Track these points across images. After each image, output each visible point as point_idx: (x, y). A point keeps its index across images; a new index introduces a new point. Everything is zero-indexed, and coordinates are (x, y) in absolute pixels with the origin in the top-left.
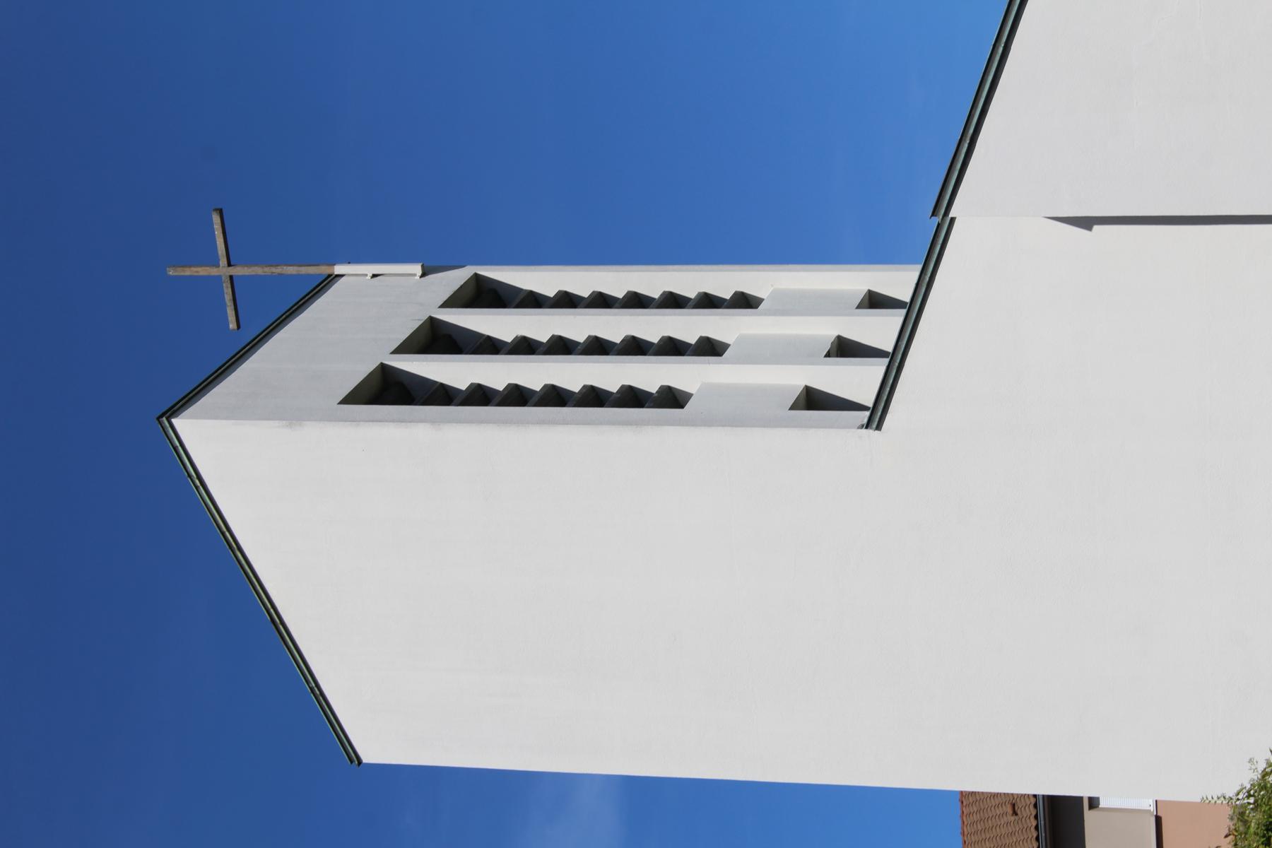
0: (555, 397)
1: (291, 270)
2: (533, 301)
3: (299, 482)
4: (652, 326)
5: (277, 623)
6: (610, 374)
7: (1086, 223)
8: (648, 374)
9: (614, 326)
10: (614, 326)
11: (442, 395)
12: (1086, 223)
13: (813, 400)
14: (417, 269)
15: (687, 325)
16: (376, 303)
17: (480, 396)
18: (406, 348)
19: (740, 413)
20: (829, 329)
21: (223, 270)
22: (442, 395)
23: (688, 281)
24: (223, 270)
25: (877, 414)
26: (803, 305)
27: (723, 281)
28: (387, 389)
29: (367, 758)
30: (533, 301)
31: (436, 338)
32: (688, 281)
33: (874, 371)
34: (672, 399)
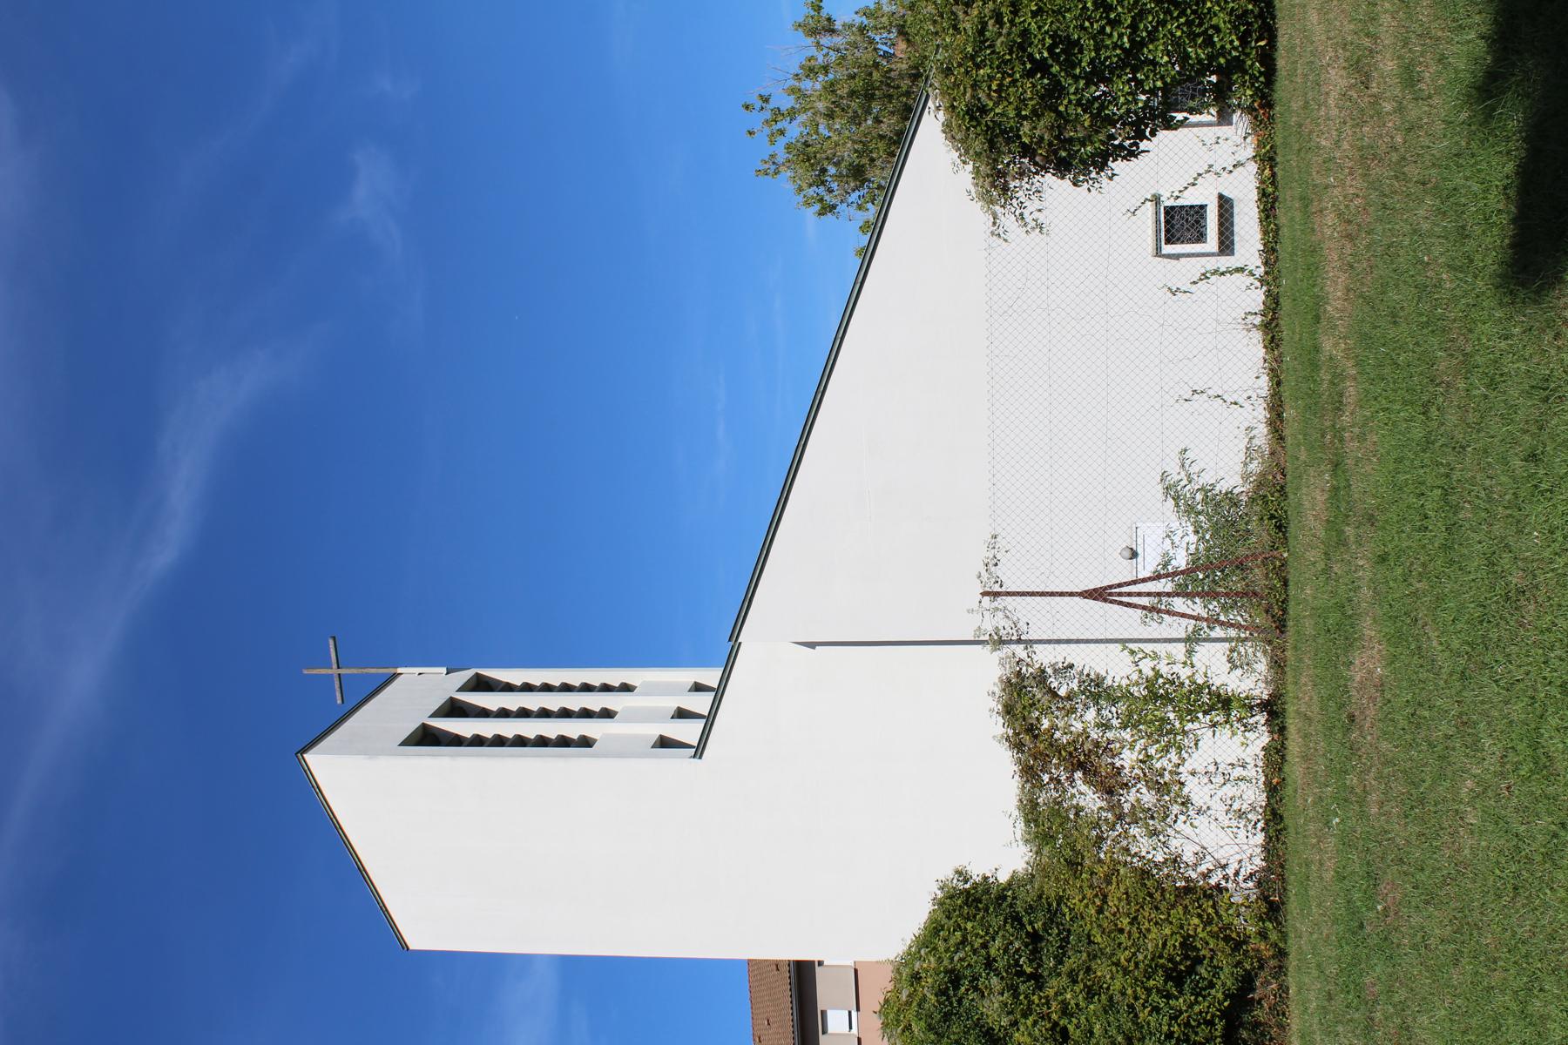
0: (520, 742)
1: (373, 671)
2: (509, 688)
3: (367, 784)
4: (575, 702)
5: (361, 870)
6: (551, 729)
7: (812, 645)
8: (573, 729)
9: (554, 702)
10: (554, 702)
11: (457, 741)
12: (812, 645)
13: (664, 743)
14: (444, 670)
15: (595, 702)
16: (420, 690)
17: (478, 741)
18: (436, 715)
19: (623, 750)
20: (673, 703)
21: (334, 671)
22: (457, 741)
23: (596, 677)
24: (334, 671)
25: (699, 750)
26: (658, 690)
27: (615, 677)
28: (426, 737)
29: (412, 947)
30: (509, 688)
31: (454, 709)
32: (596, 677)
33: (698, 725)
34: (585, 742)
